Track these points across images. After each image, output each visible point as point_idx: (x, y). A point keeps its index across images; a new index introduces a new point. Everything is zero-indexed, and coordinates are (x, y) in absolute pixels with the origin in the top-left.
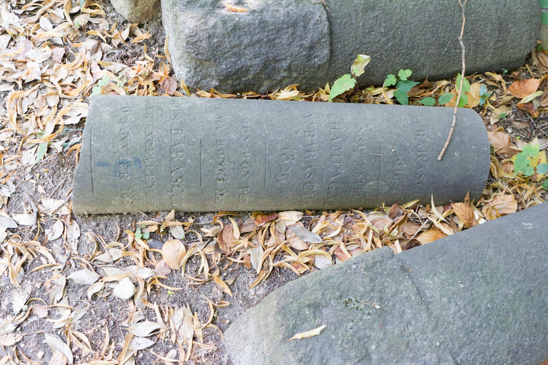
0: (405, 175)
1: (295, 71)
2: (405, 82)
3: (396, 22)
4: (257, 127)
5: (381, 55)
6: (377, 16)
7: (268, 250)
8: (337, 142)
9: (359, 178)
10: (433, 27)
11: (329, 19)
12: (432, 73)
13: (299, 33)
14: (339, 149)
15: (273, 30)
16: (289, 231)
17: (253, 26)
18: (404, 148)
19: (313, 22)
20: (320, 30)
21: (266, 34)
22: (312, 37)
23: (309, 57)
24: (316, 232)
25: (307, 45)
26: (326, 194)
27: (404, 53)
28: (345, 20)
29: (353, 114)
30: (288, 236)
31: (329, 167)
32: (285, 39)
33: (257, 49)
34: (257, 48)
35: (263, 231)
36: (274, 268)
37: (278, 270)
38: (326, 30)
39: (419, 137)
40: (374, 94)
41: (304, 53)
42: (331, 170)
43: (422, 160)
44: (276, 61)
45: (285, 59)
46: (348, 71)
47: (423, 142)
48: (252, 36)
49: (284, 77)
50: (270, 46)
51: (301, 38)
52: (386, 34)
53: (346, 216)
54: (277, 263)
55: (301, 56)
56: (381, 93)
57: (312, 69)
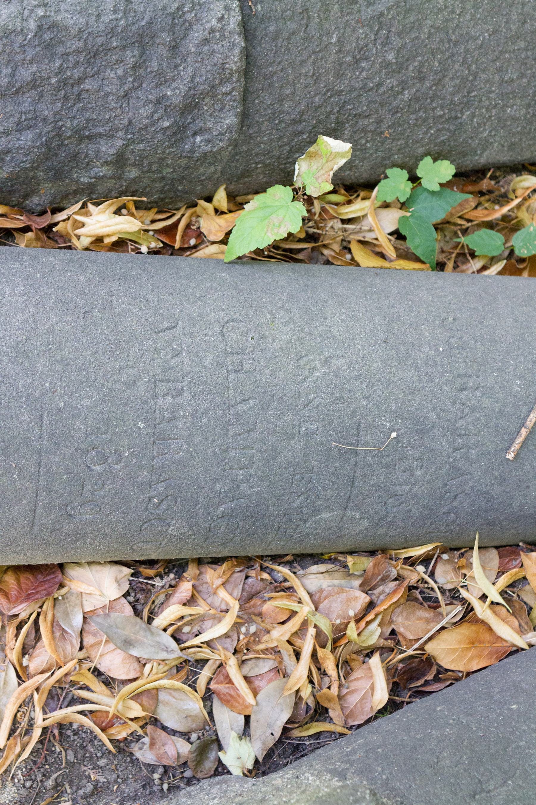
0: (416, 495)
1: (134, 165)
2: (433, 193)
3: (430, 35)
4: (18, 369)
5: (379, 121)
6: (382, 14)
7: (31, 683)
8: (245, 413)
9: (295, 505)
10: (526, 49)
11: (247, 29)
12: (505, 157)
13: (155, 65)
14: (249, 431)
15: (78, 52)
16: (92, 627)
17: (20, 38)
18: (421, 428)
19: (197, 34)
20: (217, 58)
21: (58, 63)
22: (193, 78)
23: (179, 133)
24: (165, 623)
25: (176, 100)
26: (199, 542)
27: (441, 116)
28: (292, 26)
29: (292, 320)
30: (89, 640)
31: (216, 480)
32: (112, 79)
33: (26, 105)
34: (27, 102)
35: (19, 628)
36: (45, 730)
37: (56, 732)
38: (235, 61)
39: (463, 396)
40: (345, 217)
41: (167, 124)
42: (221, 487)
43: (467, 458)
44: (81, 139)
45: (110, 136)
46: (287, 179)
47: (473, 409)
48: (15, 69)
49: (101, 178)
50: (66, 98)
51: (162, 79)
52: (401, 66)
53: (247, 577)
54: (58, 715)
55: (156, 132)
56: (365, 216)
57: (184, 162)
